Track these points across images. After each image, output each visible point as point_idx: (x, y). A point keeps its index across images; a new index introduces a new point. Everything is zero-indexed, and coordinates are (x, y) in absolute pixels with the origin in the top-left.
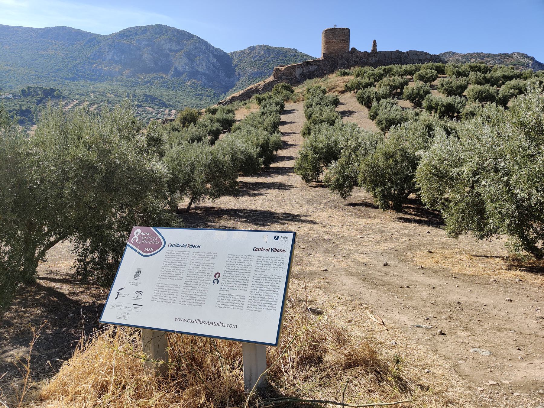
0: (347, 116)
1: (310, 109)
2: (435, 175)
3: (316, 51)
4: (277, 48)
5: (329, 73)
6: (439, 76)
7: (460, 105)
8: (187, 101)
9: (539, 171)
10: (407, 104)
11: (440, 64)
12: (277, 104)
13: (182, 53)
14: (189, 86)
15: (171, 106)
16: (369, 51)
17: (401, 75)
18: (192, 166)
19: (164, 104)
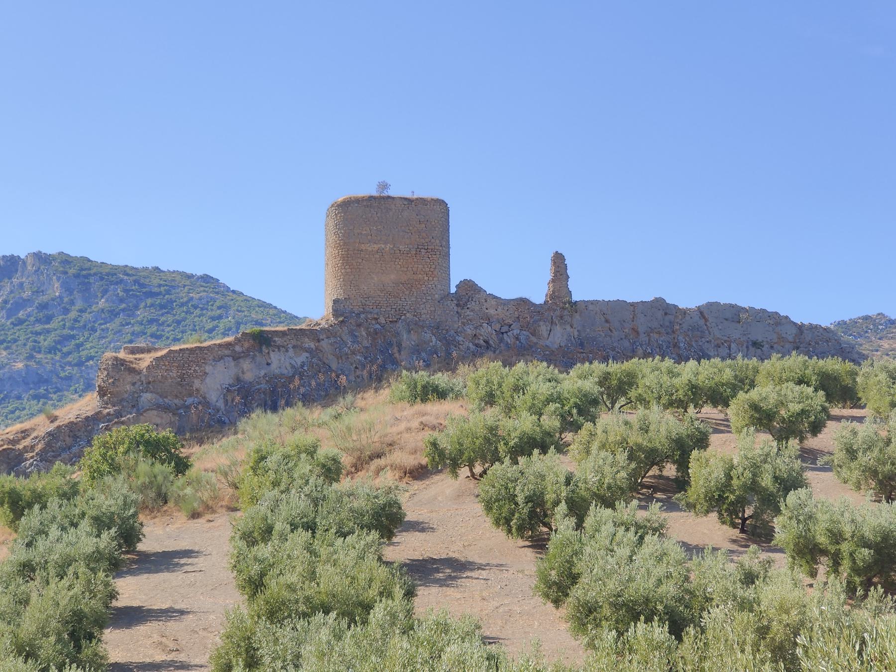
0: (442, 583)
1: (264, 551)
3: (301, 286)
4: (126, 270)
5: (359, 386)
6: (835, 411)
10: (711, 530)
11: (833, 365)
12: (101, 523)
16: (538, 295)
17: (677, 404)
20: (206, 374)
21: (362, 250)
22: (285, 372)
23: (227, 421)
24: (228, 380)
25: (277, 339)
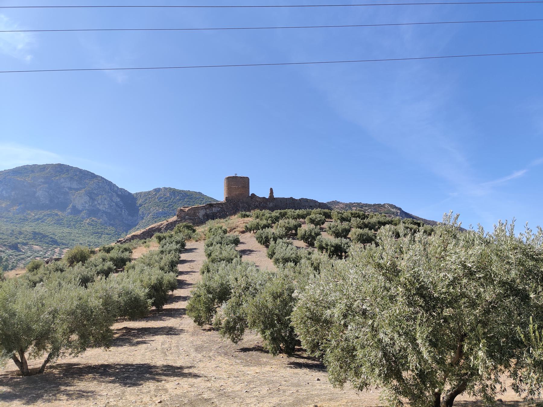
0: (247, 255)
1: (211, 248)
2: (310, 318)
3: (219, 195)
4: (183, 191)
6: (327, 220)
7: (346, 245)
8: (84, 239)
9: (400, 313)
10: (302, 244)
12: (177, 243)
13: (83, 191)
14: (88, 224)
15: (63, 244)
17: (295, 218)
18: (54, 313)
19: (55, 242)
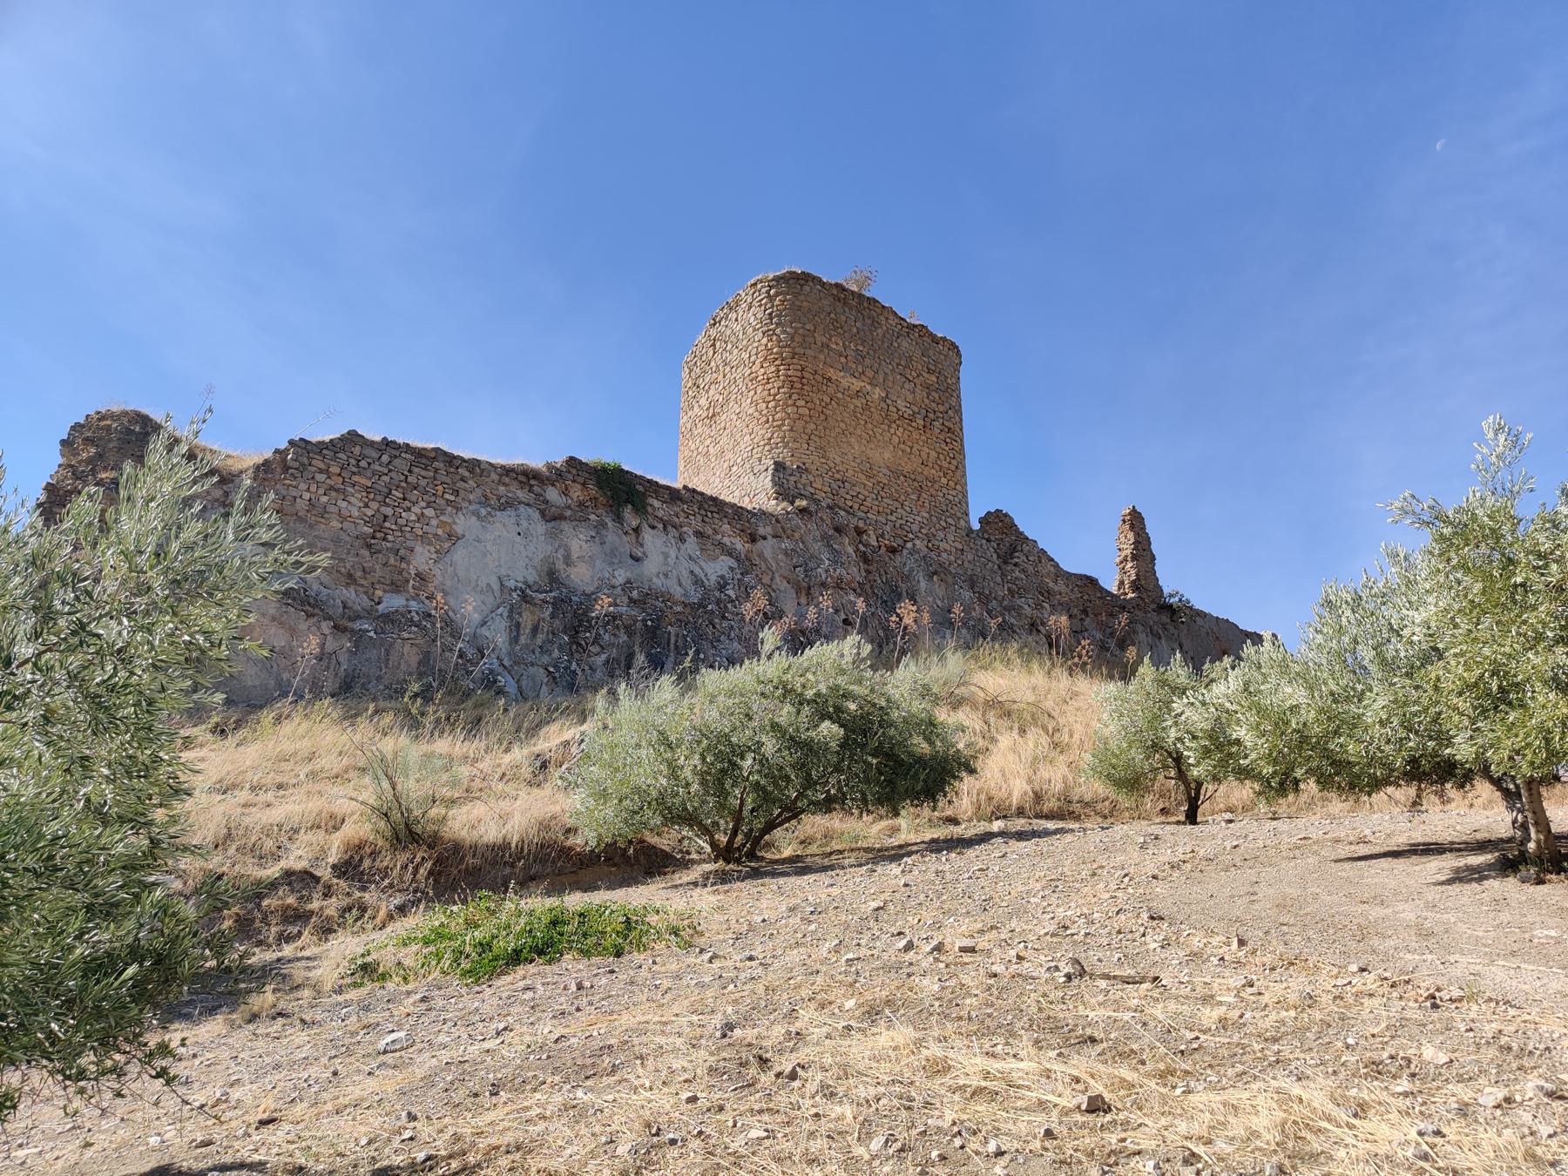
20: (453, 537)
21: (830, 380)
22: (678, 592)
23: (511, 688)
24: (523, 571)
25: (656, 503)
